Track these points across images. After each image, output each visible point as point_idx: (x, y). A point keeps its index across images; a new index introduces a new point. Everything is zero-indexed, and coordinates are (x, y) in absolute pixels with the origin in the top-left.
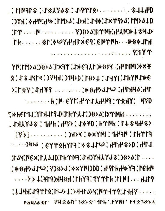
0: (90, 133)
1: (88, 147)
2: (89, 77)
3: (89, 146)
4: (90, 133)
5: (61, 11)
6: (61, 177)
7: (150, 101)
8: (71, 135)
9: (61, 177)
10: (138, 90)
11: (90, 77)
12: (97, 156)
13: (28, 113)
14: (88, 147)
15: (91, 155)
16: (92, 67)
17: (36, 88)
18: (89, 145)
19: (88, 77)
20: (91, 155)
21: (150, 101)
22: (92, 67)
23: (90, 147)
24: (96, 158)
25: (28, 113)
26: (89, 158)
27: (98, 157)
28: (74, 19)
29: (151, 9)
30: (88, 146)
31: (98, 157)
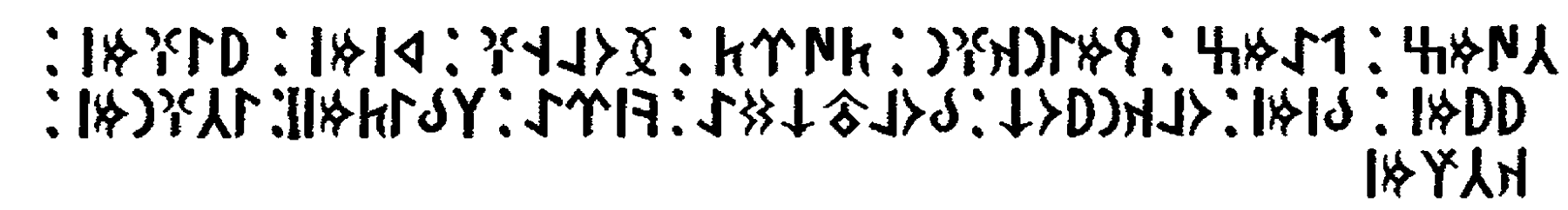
0: (118, 35)
1: (844, 133)
2: (742, 102)
3: (854, 124)
4: (118, 35)
5: (422, 122)
6: (381, 129)
7: (234, 59)
8: (1122, 109)
9: (381, 129)
10: (1337, 118)
11: (752, 103)
12: (984, 41)
13: (1326, 39)
14: (844, 133)
15: (1030, 31)
16: (227, 114)
17: (1305, 66)
18: (853, 110)
19: (732, 102)
20: (1030, 31)
21: (234, 59)
22: (227, 114)
23: (863, 130)
24: (977, 56)
25: (1326, 39)
26: (1014, 53)
27: (997, 48)
28: (53, 132)
29: (1510, 98)
30: (844, 123)
31: (997, 48)
